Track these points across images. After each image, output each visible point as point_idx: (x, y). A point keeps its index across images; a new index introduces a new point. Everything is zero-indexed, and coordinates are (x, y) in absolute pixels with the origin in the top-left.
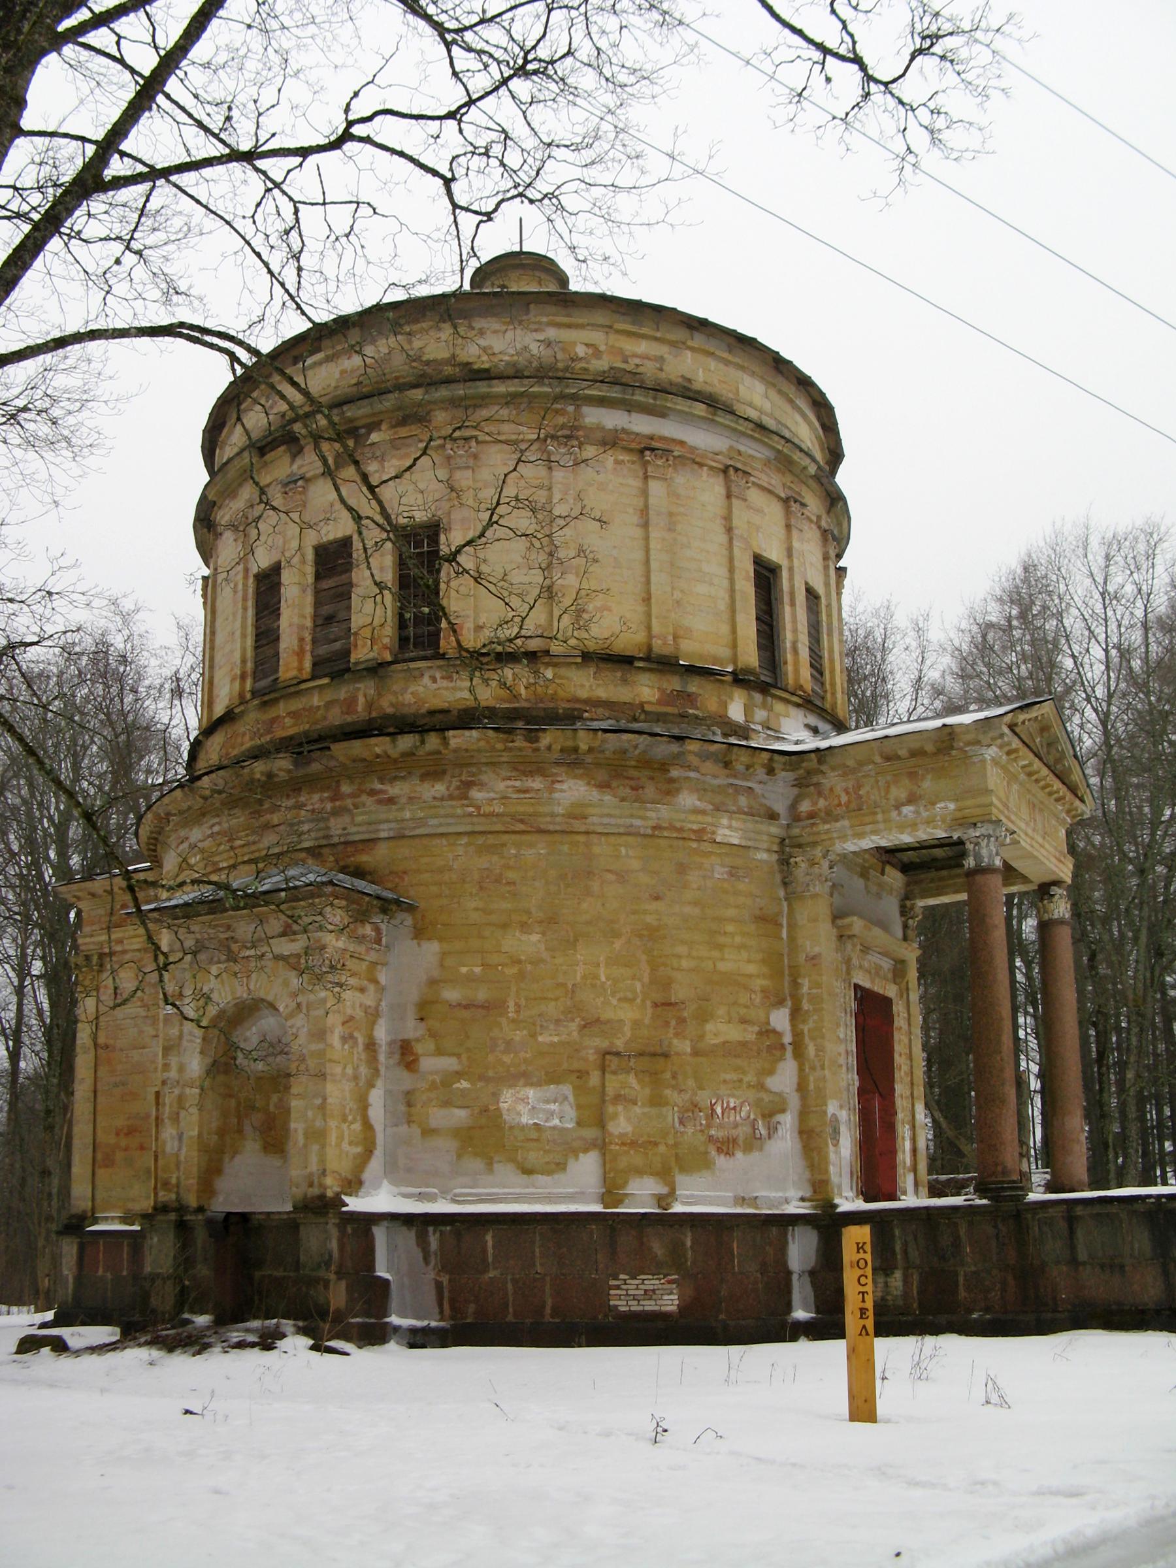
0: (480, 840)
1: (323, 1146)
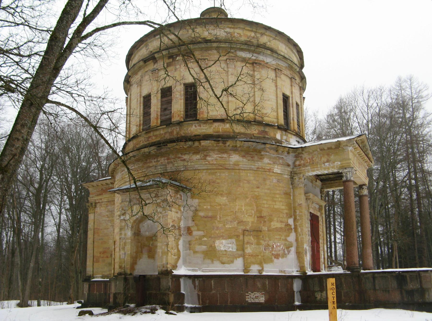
0: (210, 171)
1: (167, 256)
